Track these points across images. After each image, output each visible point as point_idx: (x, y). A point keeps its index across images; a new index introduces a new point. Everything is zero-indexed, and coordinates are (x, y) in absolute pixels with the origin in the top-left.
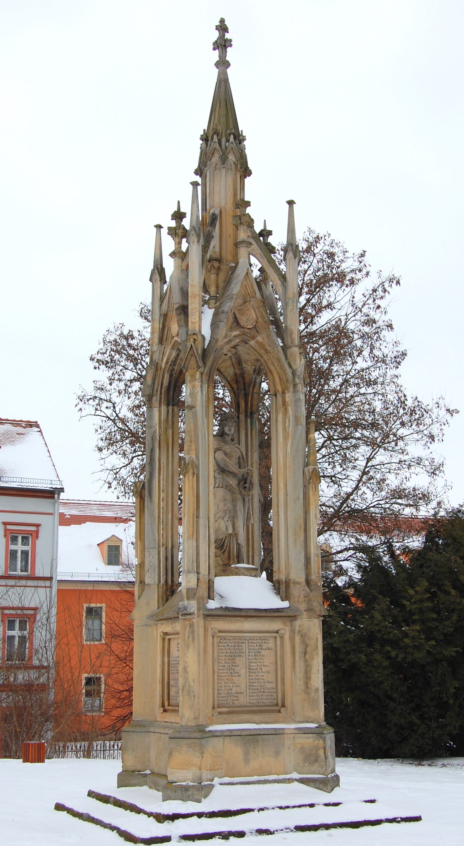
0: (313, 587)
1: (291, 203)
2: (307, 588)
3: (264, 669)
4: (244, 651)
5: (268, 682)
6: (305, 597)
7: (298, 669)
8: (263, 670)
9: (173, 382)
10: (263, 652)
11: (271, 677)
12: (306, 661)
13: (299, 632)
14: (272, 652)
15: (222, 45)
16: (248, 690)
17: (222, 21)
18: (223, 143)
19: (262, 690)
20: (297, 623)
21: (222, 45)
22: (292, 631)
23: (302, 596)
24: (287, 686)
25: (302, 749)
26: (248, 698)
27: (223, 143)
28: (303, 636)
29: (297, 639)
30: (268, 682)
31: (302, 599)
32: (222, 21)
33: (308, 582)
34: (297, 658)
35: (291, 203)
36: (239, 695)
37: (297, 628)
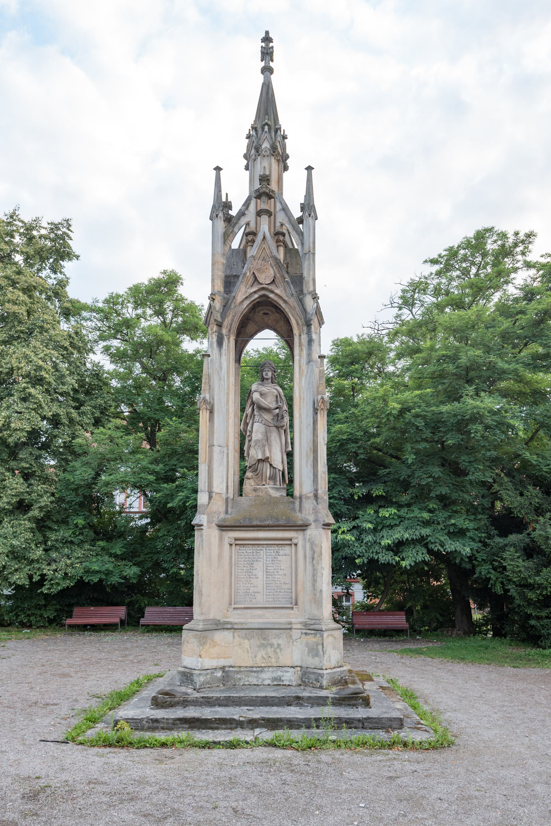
0: (319, 501)
1: (218, 169)
2: (315, 502)
3: (281, 572)
4: (262, 557)
5: (284, 583)
6: (313, 509)
7: (308, 570)
8: (280, 573)
9: (312, 269)
10: (280, 558)
11: (288, 580)
12: (314, 566)
13: (309, 540)
14: (288, 558)
15: (267, 54)
16: (265, 590)
17: (267, 33)
18: (266, 138)
19: (278, 590)
20: (309, 532)
21: (267, 54)
22: (305, 539)
23: (311, 509)
24: (300, 588)
25: (307, 644)
26: (265, 597)
27: (266, 138)
28: (312, 544)
29: (308, 545)
30: (284, 583)
31: (311, 512)
32: (267, 33)
33: (316, 496)
34: (307, 563)
35: (218, 169)
36: (256, 594)
37: (308, 537)
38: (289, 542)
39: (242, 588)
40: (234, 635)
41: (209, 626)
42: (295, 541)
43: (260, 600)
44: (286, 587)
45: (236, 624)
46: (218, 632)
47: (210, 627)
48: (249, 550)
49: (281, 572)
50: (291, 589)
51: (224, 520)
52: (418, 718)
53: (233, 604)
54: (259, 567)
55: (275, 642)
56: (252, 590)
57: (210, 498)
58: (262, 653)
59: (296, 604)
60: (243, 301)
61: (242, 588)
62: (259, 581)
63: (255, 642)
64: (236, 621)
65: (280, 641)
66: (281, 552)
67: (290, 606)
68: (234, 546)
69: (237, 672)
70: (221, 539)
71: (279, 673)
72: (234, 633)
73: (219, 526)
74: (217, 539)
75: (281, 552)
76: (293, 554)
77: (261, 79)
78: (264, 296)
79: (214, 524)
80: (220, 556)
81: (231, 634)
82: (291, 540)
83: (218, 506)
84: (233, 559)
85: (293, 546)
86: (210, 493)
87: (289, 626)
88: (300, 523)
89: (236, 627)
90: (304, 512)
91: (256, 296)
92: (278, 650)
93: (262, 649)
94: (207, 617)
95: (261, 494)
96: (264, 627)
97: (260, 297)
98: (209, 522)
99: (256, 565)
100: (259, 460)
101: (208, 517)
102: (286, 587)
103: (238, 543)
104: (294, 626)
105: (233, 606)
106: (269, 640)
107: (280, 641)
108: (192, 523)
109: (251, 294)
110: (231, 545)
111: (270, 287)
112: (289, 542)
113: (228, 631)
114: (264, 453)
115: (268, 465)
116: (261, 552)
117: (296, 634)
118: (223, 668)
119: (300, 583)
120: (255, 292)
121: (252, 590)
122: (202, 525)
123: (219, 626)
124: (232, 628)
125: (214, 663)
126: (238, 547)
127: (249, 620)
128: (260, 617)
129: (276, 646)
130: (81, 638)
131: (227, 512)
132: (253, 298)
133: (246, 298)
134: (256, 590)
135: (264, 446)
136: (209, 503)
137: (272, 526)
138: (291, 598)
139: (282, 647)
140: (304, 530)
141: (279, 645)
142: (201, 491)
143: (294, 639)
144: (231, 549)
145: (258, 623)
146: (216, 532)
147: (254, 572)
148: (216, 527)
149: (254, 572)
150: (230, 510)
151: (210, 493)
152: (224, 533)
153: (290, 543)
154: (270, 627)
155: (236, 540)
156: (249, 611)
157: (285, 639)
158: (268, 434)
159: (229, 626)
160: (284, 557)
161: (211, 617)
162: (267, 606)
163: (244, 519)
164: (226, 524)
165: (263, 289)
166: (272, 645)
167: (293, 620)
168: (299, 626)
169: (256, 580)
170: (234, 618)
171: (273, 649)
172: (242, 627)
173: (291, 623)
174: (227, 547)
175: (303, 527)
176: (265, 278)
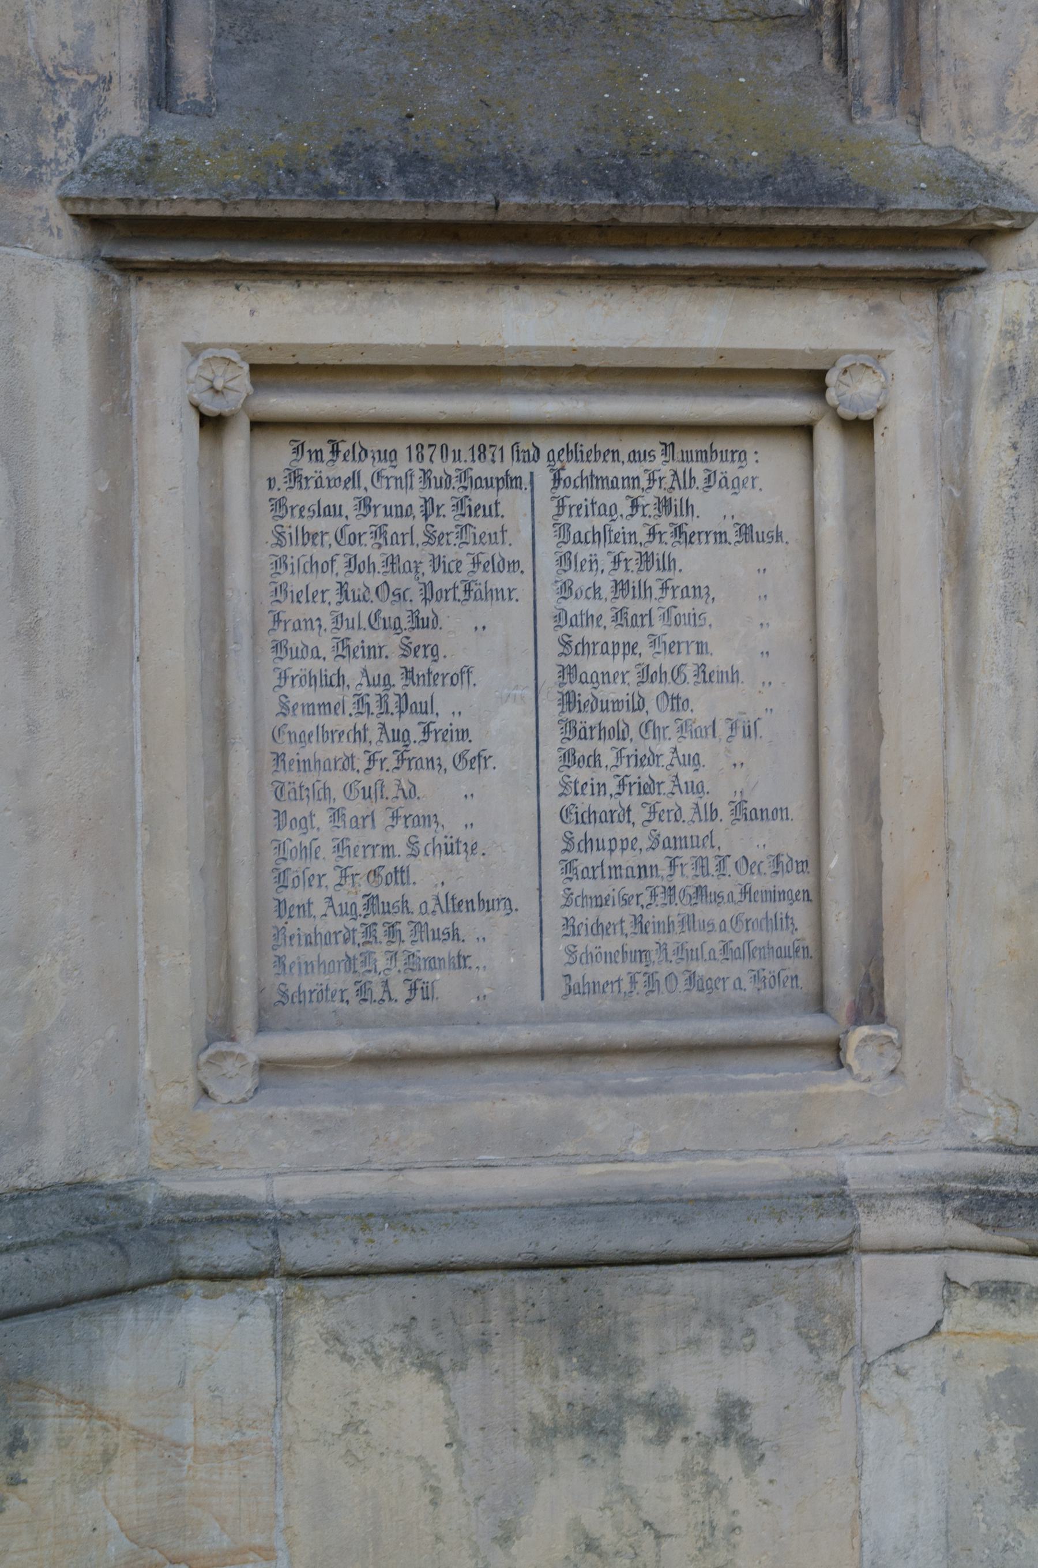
3: (705, 703)
4: (518, 551)
5: (744, 812)
8: (699, 714)
10: (693, 563)
11: (779, 782)
13: (1007, 376)
14: (784, 562)
16: (553, 875)
22: (953, 377)
24: (904, 849)
26: (556, 948)
30: (744, 812)
34: (989, 608)
36: (469, 923)
37: (991, 348)
38: (794, 408)
39: (325, 865)
40: (283, 1339)
41: (47, 1259)
42: (852, 393)
43: (508, 972)
44: (756, 841)
46: (130, 1316)
48: (393, 480)
49: (705, 703)
50: (815, 863)
52: (109, 1224)
55: (697, 1379)
56: (428, 875)
59: (870, 1005)
61: (325, 865)
62: (497, 809)
64: (300, 1190)
65: (748, 1376)
66: (710, 508)
67: (810, 1026)
68: (237, 441)
70: (115, 352)
72: (280, 1313)
73: (97, 224)
74: (81, 356)
75: (710, 508)
76: (831, 524)
79: (48, 197)
81: (259, 1321)
82: (814, 381)
84: (238, 576)
85: (829, 442)
87: (826, 1230)
88: (916, 203)
89: (301, 1250)
90: (944, 107)
92: (726, 1460)
93: (567, 1451)
99: (457, 627)
102: (756, 841)
103: (280, 407)
104: (873, 1228)
105: (254, 1047)
106: (630, 1369)
107: (748, 1376)
110: (212, 424)
112: (794, 408)
113: (229, 1299)
116: (514, 501)
117: (887, 1296)
119: (903, 810)
121: (428, 875)
124: (250, 1251)
126: (279, 454)
127: (424, 1184)
128: (532, 1145)
129: (704, 1422)
131: (161, 87)
134: (465, 877)
137: (643, 236)
138: (818, 955)
139: (760, 1424)
140: (942, 282)
141: (732, 1413)
143: (877, 1342)
144: (212, 472)
147: (448, 703)
148: (68, 238)
149: (448, 703)
150: (193, 62)
152: (145, 301)
155: (266, 372)
156: (419, 1088)
157: (795, 1351)
159: (233, 1250)
160: (739, 559)
161: (51, 1162)
162: (592, 1033)
164: (179, 202)
166: (666, 1416)
167: (857, 1167)
168: (923, 1223)
169: (464, 779)
170: (265, 1158)
171: (675, 1451)
172: (360, 1255)
173: (836, 1197)
174: (169, 442)
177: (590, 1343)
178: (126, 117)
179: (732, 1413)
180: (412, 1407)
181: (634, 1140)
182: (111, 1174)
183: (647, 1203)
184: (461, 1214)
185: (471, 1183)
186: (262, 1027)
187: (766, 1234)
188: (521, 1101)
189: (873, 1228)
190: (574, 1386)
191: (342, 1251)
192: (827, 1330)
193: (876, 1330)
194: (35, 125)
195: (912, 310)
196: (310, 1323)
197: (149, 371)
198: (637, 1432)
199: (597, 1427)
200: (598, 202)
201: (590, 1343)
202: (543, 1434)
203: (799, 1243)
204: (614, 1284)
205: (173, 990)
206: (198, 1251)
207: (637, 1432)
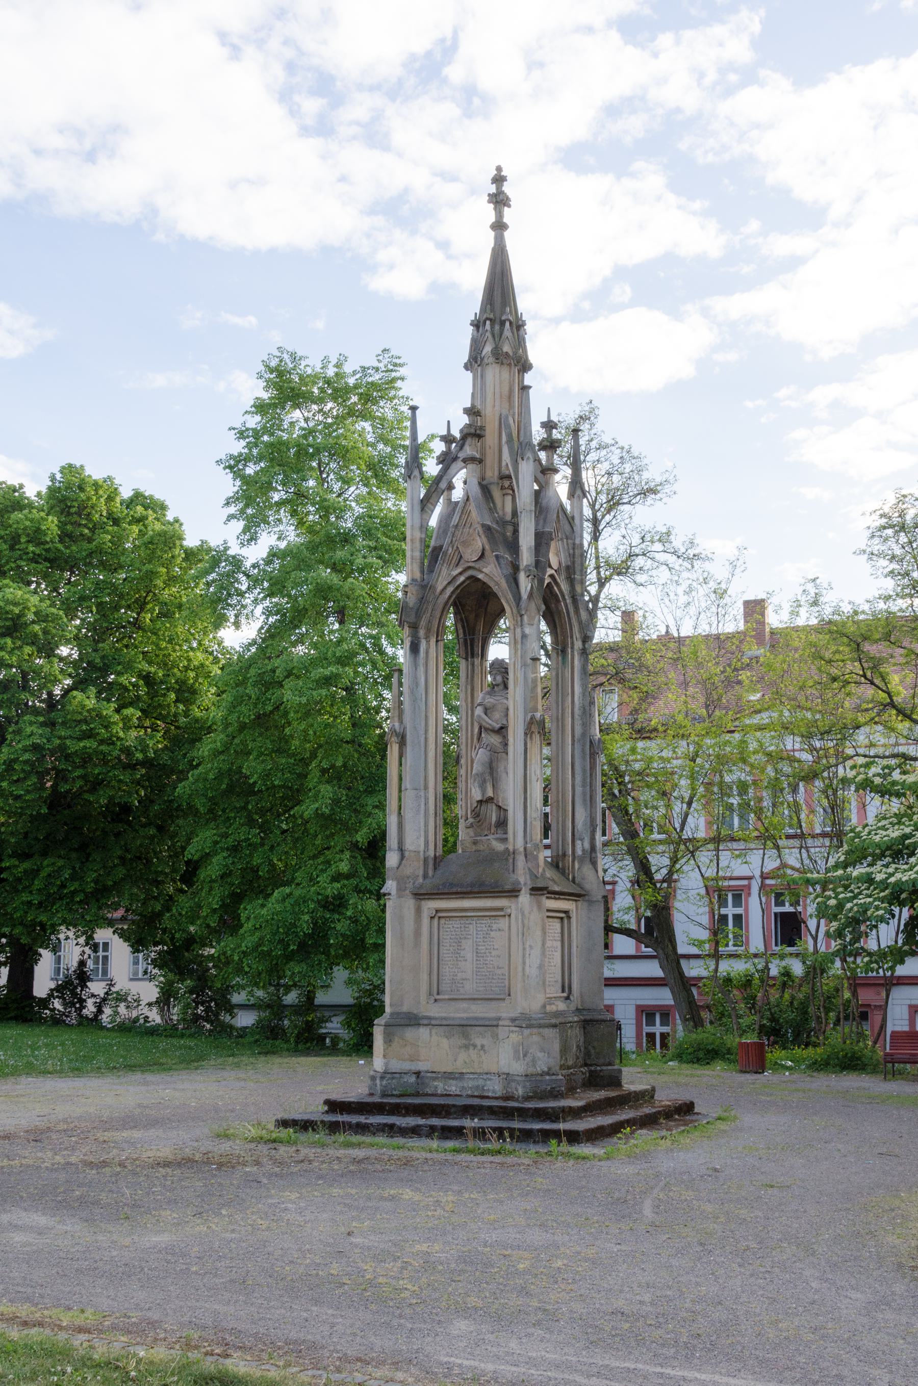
3: (494, 953)
5: (498, 968)
8: (493, 954)
10: (492, 934)
26: (475, 985)
30: (498, 968)
36: (465, 982)
38: (502, 913)
43: (469, 988)
44: (499, 972)
45: (436, 1019)
47: (403, 1022)
49: (494, 953)
51: (421, 886)
53: (436, 993)
54: (468, 945)
55: (479, 1042)
57: (402, 857)
58: (463, 1056)
59: (509, 995)
60: (445, 588)
63: (459, 1041)
64: (437, 1015)
65: (485, 1042)
69: (434, 1079)
70: (418, 910)
71: (481, 1082)
74: (413, 911)
75: (495, 927)
77: (490, 237)
78: (471, 577)
79: (408, 892)
80: (417, 933)
81: (428, 1031)
82: (501, 909)
83: (414, 868)
86: (401, 850)
87: (495, 1023)
89: (433, 1022)
91: (462, 578)
92: (482, 1052)
93: (463, 1050)
94: (397, 1010)
95: (482, 848)
96: (465, 1023)
97: (468, 578)
98: (400, 890)
100: (480, 802)
101: (398, 883)
102: (499, 972)
104: (501, 1023)
106: (470, 1040)
108: (382, 891)
109: (457, 575)
111: (477, 565)
114: (484, 791)
115: (494, 807)
116: (471, 926)
117: (502, 1032)
118: (418, 1074)
120: (461, 573)
122: (389, 894)
123: (413, 1020)
125: (407, 1066)
127: (452, 1015)
129: (479, 1047)
130: (686, 1140)
131: (425, 876)
132: (458, 583)
133: (449, 583)
135: (484, 781)
136: (400, 864)
139: (486, 1048)
141: (483, 1046)
142: (390, 849)
145: (462, 1019)
146: (410, 903)
147: (462, 953)
148: (411, 896)
149: (462, 953)
150: (430, 873)
151: (401, 850)
152: (423, 902)
153: (500, 913)
154: (473, 1023)
155: (437, 911)
157: (491, 1039)
158: (494, 764)
159: (425, 1022)
163: (444, 884)
164: (422, 891)
165: (469, 568)
166: (475, 1046)
174: (426, 921)
175: (514, 893)
176: (470, 555)
177: (466, 1036)
178: (421, 880)
179: (483, 1046)
180: (445, 1042)
181: (478, 1011)
182: (415, 1012)
183: (476, 1019)
184: (453, 1019)
185: (458, 1015)
186: (438, 994)
187: (487, 1023)
188: (464, 1005)
189: (501, 1023)
190: (464, 1041)
191: (438, 1022)
192: (495, 1037)
193: (501, 1037)
194: (406, 883)
195: (513, 899)
196: (434, 1031)
197: (507, 582)
198: (471, 1048)
199: (466, 1047)
200: (469, 889)
201: (466, 1036)
202: (460, 1047)
203: (492, 1025)
204: (469, 1028)
205: (424, 988)
206: (421, 1022)
207: (471, 1048)
